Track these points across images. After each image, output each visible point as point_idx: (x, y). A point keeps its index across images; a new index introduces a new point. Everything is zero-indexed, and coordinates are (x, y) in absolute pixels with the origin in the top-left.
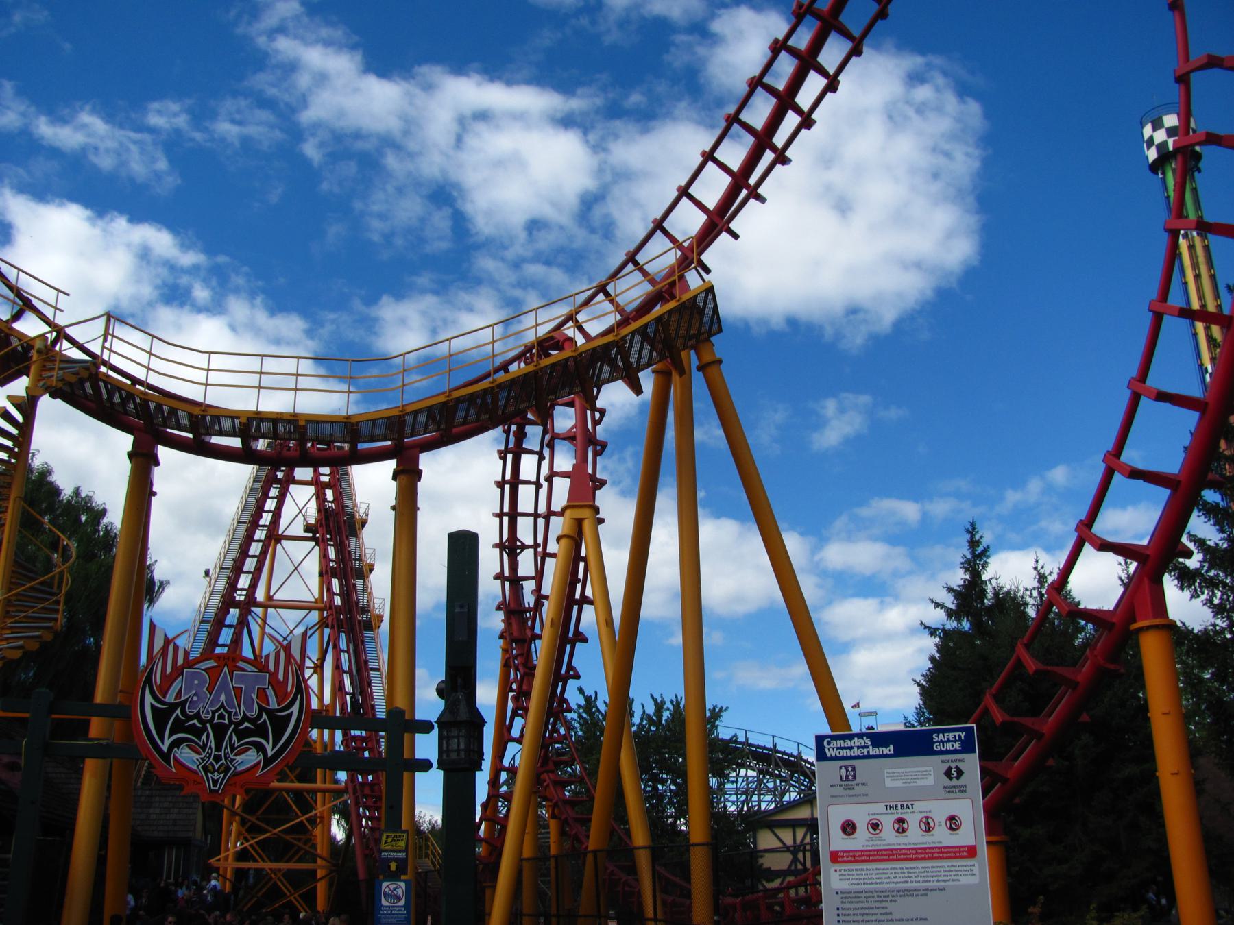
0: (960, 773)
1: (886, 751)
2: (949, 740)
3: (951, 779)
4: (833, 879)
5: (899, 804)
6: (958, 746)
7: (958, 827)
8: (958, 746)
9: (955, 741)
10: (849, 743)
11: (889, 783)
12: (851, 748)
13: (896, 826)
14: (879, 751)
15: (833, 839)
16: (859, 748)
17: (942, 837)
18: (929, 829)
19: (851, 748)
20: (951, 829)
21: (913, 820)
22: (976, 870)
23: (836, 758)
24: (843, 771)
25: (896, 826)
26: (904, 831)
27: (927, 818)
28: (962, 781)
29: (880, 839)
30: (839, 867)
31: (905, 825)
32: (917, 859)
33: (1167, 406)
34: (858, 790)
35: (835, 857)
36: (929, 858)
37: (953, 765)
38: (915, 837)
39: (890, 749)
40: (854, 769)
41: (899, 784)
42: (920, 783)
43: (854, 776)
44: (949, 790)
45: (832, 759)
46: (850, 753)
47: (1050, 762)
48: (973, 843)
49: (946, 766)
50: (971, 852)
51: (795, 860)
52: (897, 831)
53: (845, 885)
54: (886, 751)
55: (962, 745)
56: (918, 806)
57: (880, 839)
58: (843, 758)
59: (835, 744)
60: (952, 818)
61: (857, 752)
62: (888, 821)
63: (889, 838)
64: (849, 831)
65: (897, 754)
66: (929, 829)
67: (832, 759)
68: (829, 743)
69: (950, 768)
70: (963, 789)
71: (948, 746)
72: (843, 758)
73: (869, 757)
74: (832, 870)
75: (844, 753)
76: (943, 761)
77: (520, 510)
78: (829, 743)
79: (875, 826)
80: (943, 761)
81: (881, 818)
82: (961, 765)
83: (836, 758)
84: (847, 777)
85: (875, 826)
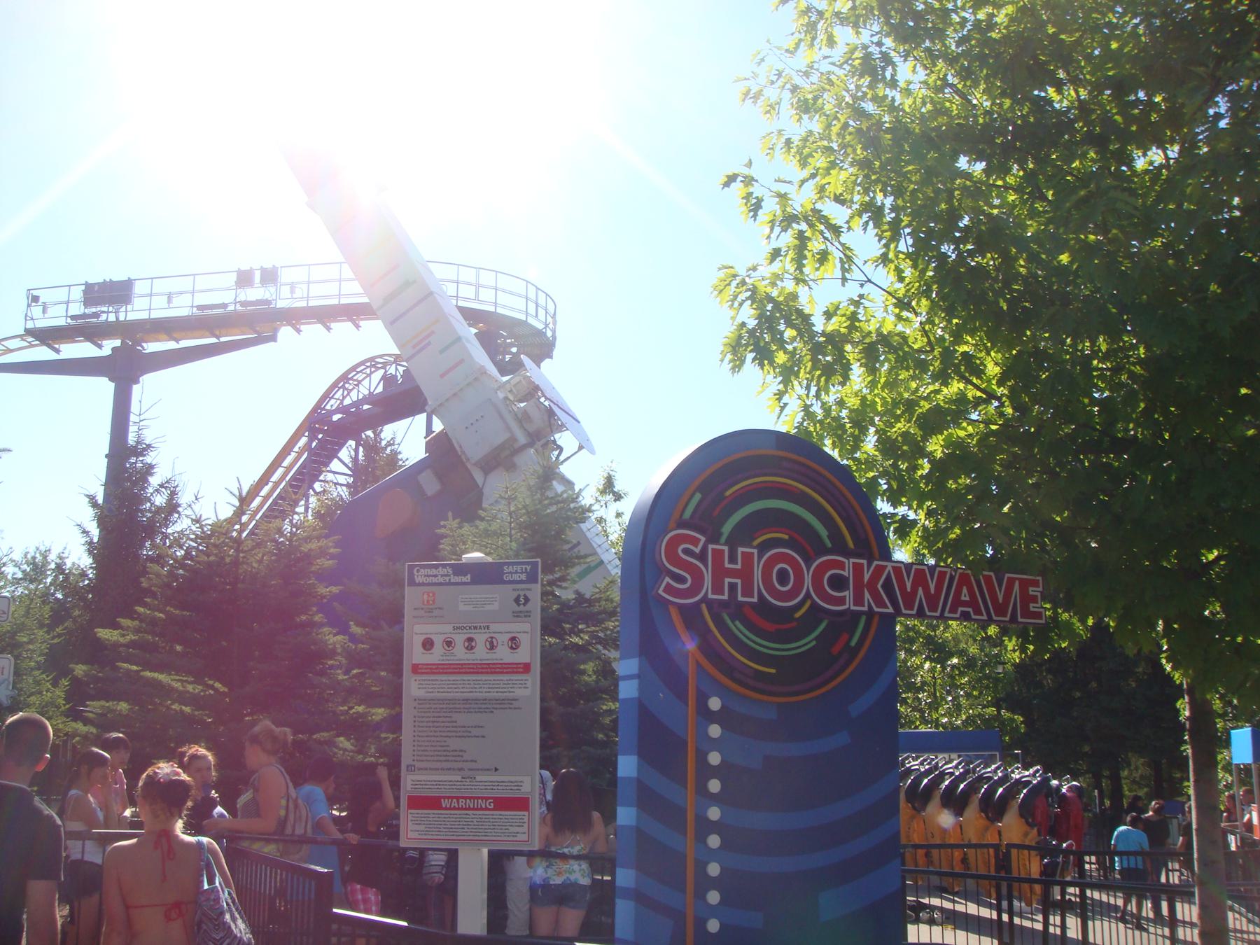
0: (527, 600)
1: (464, 579)
2: (516, 572)
4: (414, 688)
6: (523, 577)
7: (518, 647)
8: (523, 577)
11: (462, 607)
12: (435, 576)
15: (415, 654)
17: (503, 654)
18: (492, 647)
19: (435, 576)
20: (512, 648)
21: (480, 639)
22: (529, 684)
23: (510, 582)
26: (472, 648)
28: (529, 607)
30: (418, 677)
33: (220, 293)
35: (416, 669)
38: (481, 653)
39: (468, 578)
41: (470, 608)
42: (489, 607)
44: (517, 615)
46: (435, 580)
49: (516, 594)
50: (526, 668)
51: (987, 687)
53: (421, 693)
54: (464, 579)
58: (428, 584)
60: (513, 639)
61: (441, 580)
62: (459, 639)
63: (460, 654)
66: (492, 647)
70: (528, 614)
71: (516, 577)
72: (428, 584)
73: (450, 584)
75: (429, 580)
79: (449, 643)
81: (432, 637)
82: (528, 593)
83: (423, 584)
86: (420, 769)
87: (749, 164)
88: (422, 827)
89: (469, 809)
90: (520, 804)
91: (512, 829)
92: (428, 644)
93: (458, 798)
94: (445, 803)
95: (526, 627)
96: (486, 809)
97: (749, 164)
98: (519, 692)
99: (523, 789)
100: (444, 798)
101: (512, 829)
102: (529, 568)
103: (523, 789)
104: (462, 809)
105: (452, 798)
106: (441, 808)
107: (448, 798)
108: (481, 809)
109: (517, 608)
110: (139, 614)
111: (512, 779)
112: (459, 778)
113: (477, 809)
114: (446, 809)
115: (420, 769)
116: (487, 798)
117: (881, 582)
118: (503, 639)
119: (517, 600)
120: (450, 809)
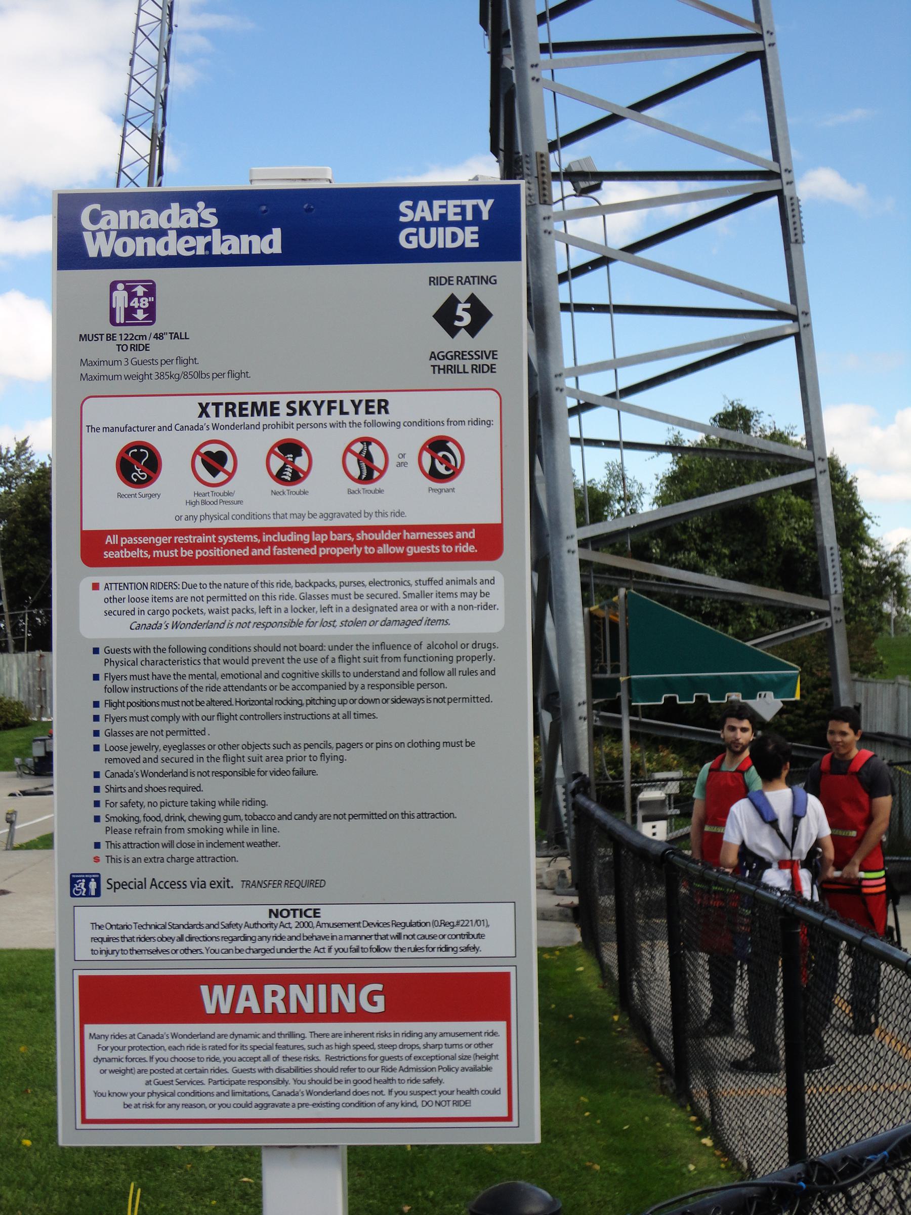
1: (260, 245)
2: (443, 222)
3: (453, 332)
5: (284, 400)
6: (469, 238)
8: (469, 238)
9: (462, 225)
10: (154, 219)
13: (277, 463)
14: (239, 244)
16: (181, 233)
17: (407, 498)
18: (369, 474)
19: (158, 233)
20: (434, 475)
21: (326, 444)
22: (497, 594)
24: (121, 297)
25: (277, 463)
26: (297, 477)
27: (367, 441)
28: (486, 338)
29: (228, 499)
30: (104, 576)
31: (301, 462)
32: (330, 559)
34: (158, 350)
35: (95, 548)
36: (365, 558)
37: (462, 293)
38: (328, 495)
39: (272, 242)
40: (151, 290)
43: (151, 312)
44: (445, 364)
45: (101, 263)
46: (155, 248)
47: (854, 833)
48: (494, 518)
49: (440, 295)
50: (487, 542)
52: (278, 477)
53: (118, 631)
54: (260, 245)
55: (482, 237)
56: (402, 406)
57: (228, 499)
58: (134, 262)
59: (115, 219)
60: (437, 445)
61: (177, 247)
62: (252, 445)
63: (253, 497)
64: (139, 473)
65: (292, 255)
66: (369, 474)
67: (101, 263)
68: (95, 218)
69: (452, 302)
70: (485, 362)
71: (441, 238)
73: (209, 260)
74: (86, 584)
75: (137, 247)
76: (434, 281)
77: (610, 357)
78: (95, 218)
79: (215, 462)
80: (434, 281)
82: (485, 295)
83: (114, 262)
84: (130, 312)
85: (215, 462)
86: (116, 886)
87: (725, 397)
88: (135, 1083)
89: (301, 1016)
90: (482, 996)
91: (451, 1081)
92: (139, 465)
93: (259, 982)
94: (214, 999)
95: (485, 404)
96: (360, 1016)
97: (725, 397)
98: (466, 624)
99: (487, 948)
100: (211, 981)
101: (451, 1081)
102: (485, 208)
103: (487, 948)
104: (275, 1017)
105: (239, 981)
106: (201, 1017)
107: (224, 981)
108: (342, 1016)
109: (440, 339)
110: (840, 765)
111: (452, 913)
112: (261, 914)
113: (329, 1017)
114: (218, 1017)
115: (116, 886)
116: (361, 981)
117: (668, 695)
118: (403, 444)
119: (446, 316)
120: (232, 1017)
